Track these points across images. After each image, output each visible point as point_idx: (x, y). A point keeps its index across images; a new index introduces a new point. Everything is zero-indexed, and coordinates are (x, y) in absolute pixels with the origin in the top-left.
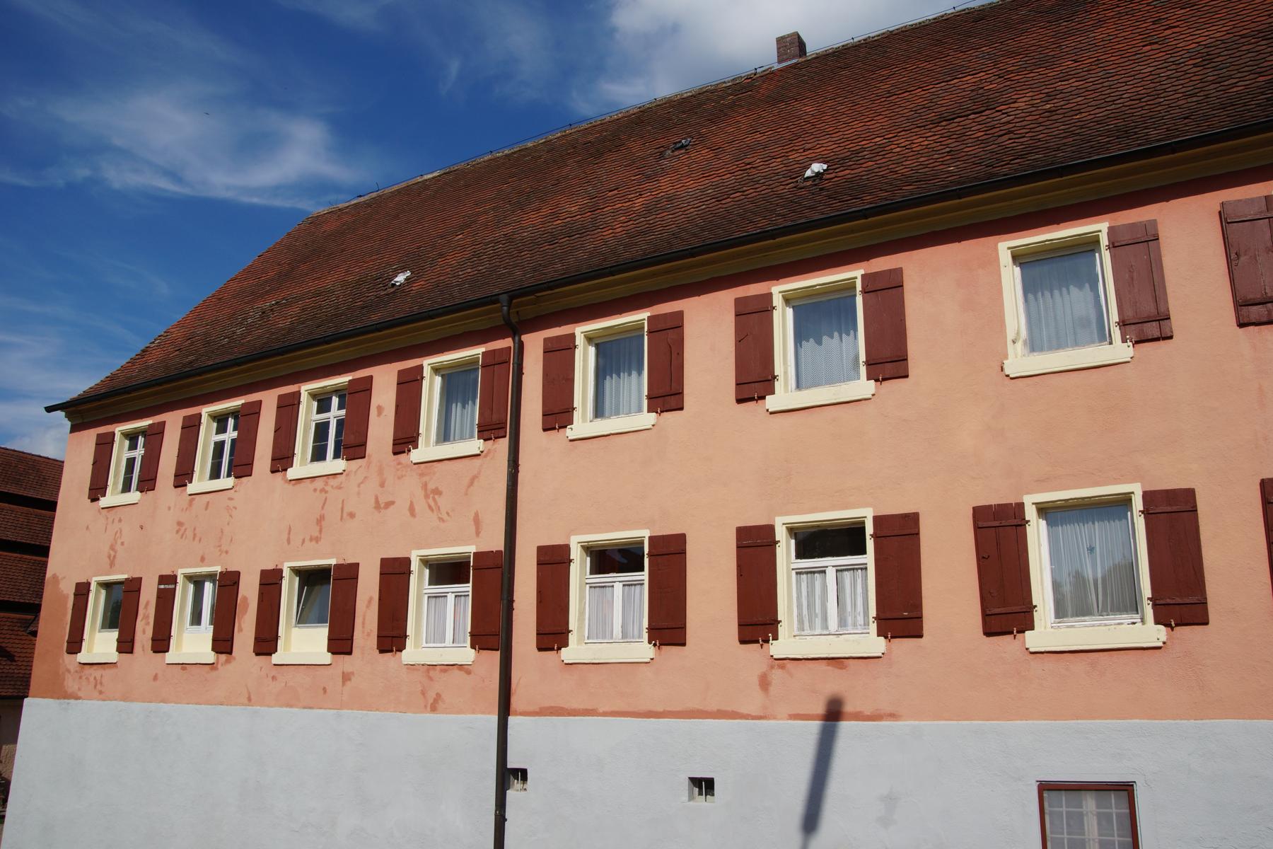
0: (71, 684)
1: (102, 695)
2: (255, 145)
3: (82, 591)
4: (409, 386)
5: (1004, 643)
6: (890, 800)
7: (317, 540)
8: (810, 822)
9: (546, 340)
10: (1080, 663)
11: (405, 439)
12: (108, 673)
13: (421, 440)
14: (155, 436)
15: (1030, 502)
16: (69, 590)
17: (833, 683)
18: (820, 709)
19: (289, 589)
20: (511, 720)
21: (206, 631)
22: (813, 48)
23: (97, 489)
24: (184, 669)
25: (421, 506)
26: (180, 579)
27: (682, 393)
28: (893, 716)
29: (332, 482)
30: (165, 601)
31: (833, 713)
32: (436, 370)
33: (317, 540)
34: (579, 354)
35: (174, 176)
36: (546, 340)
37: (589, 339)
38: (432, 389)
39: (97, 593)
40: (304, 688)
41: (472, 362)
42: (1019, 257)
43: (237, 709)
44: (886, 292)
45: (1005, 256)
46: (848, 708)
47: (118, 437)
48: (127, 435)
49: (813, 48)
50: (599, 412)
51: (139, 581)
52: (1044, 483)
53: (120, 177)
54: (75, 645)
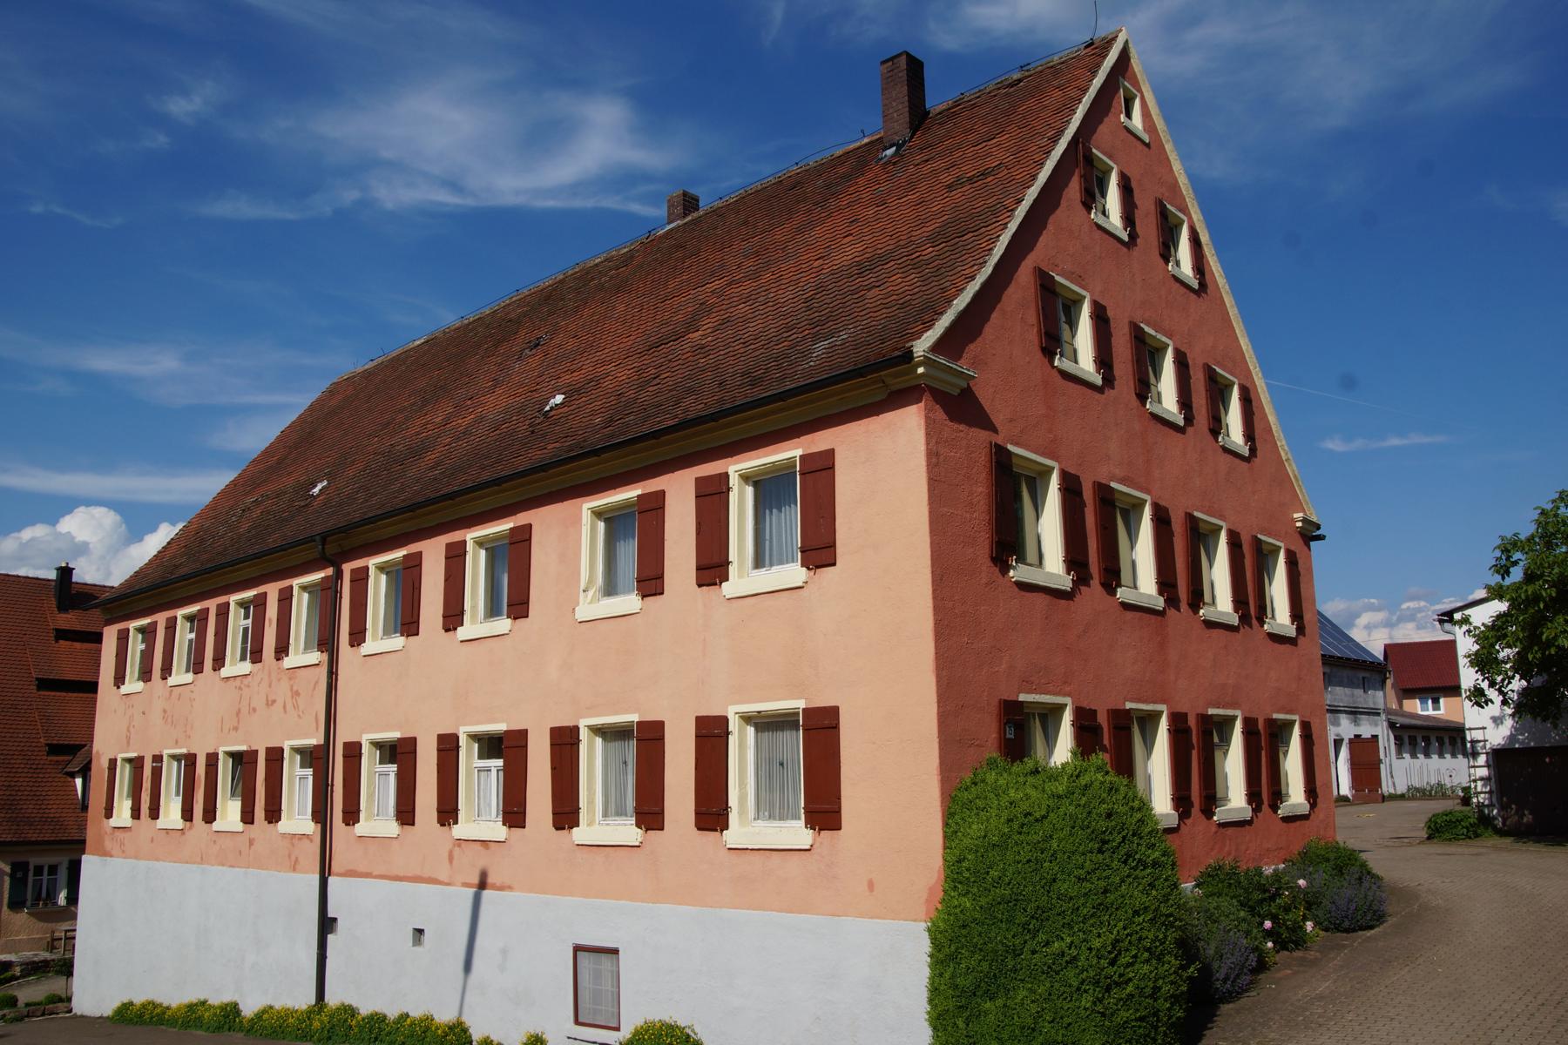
0: (108, 844)
1: (124, 854)
2: (544, 137)
3: (113, 762)
4: (712, 497)
5: (711, 836)
6: (504, 952)
7: (236, 729)
8: (468, 966)
9: (699, 481)
10: (600, 855)
11: (712, 569)
12: (127, 835)
13: (467, 617)
14: (260, 603)
15: (583, 724)
16: (105, 764)
17: (482, 859)
18: (476, 880)
19: (742, 749)
20: (331, 880)
21: (128, 804)
22: (707, 200)
23: (119, 679)
24: (487, 848)
25: (290, 706)
26: (165, 758)
27: (834, 545)
28: (510, 888)
29: (246, 681)
30: (157, 774)
31: (483, 885)
32: (480, 543)
33: (236, 729)
34: (733, 497)
35: (454, 186)
36: (699, 481)
37: (746, 478)
38: (741, 501)
39: (169, 766)
40: (233, 854)
41: (790, 463)
42: (598, 514)
43: (194, 867)
44: (821, 468)
45: (586, 516)
46: (490, 880)
47: (470, 546)
48: (242, 604)
49: (707, 200)
50: (759, 563)
51: (523, 734)
52: (592, 710)
53: (393, 195)
54: (109, 813)
